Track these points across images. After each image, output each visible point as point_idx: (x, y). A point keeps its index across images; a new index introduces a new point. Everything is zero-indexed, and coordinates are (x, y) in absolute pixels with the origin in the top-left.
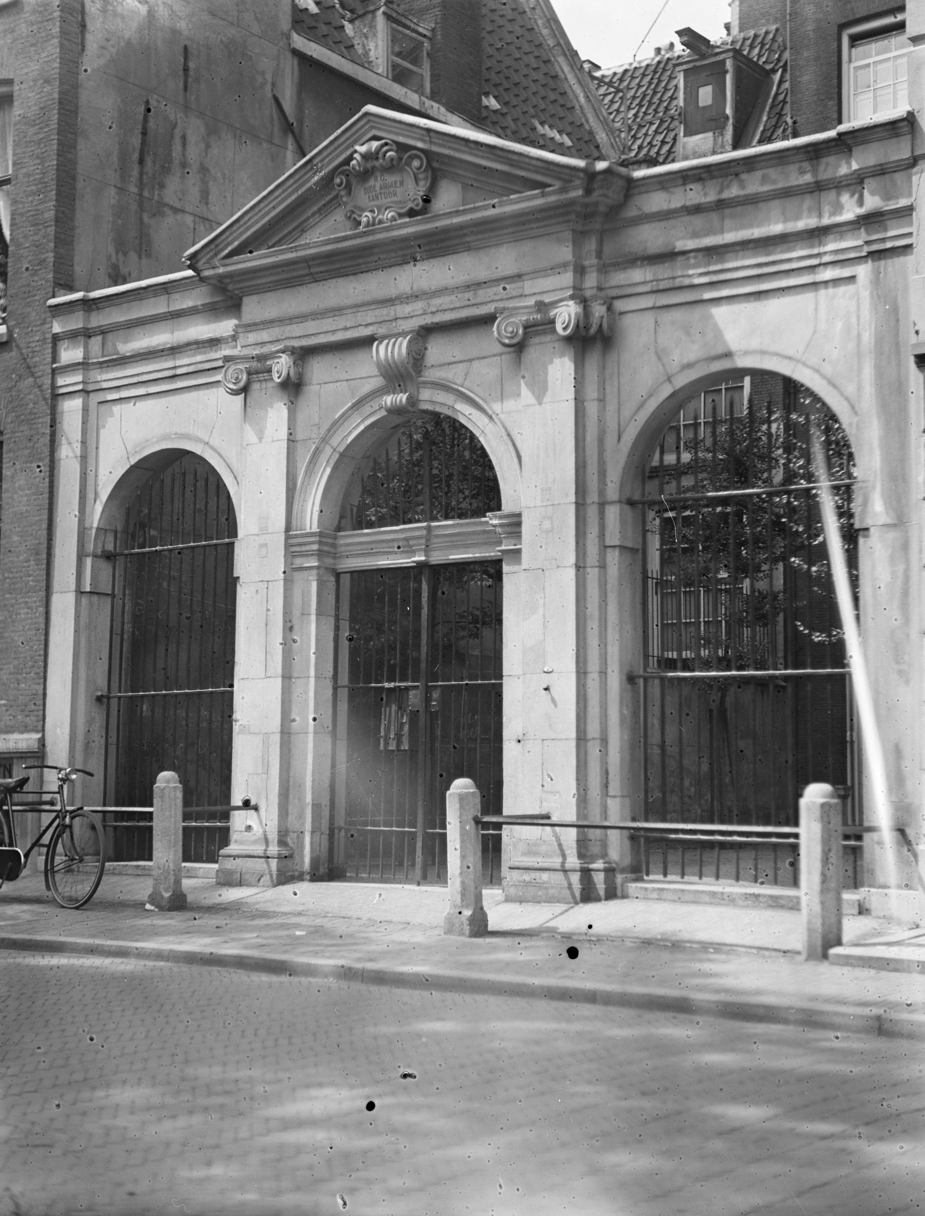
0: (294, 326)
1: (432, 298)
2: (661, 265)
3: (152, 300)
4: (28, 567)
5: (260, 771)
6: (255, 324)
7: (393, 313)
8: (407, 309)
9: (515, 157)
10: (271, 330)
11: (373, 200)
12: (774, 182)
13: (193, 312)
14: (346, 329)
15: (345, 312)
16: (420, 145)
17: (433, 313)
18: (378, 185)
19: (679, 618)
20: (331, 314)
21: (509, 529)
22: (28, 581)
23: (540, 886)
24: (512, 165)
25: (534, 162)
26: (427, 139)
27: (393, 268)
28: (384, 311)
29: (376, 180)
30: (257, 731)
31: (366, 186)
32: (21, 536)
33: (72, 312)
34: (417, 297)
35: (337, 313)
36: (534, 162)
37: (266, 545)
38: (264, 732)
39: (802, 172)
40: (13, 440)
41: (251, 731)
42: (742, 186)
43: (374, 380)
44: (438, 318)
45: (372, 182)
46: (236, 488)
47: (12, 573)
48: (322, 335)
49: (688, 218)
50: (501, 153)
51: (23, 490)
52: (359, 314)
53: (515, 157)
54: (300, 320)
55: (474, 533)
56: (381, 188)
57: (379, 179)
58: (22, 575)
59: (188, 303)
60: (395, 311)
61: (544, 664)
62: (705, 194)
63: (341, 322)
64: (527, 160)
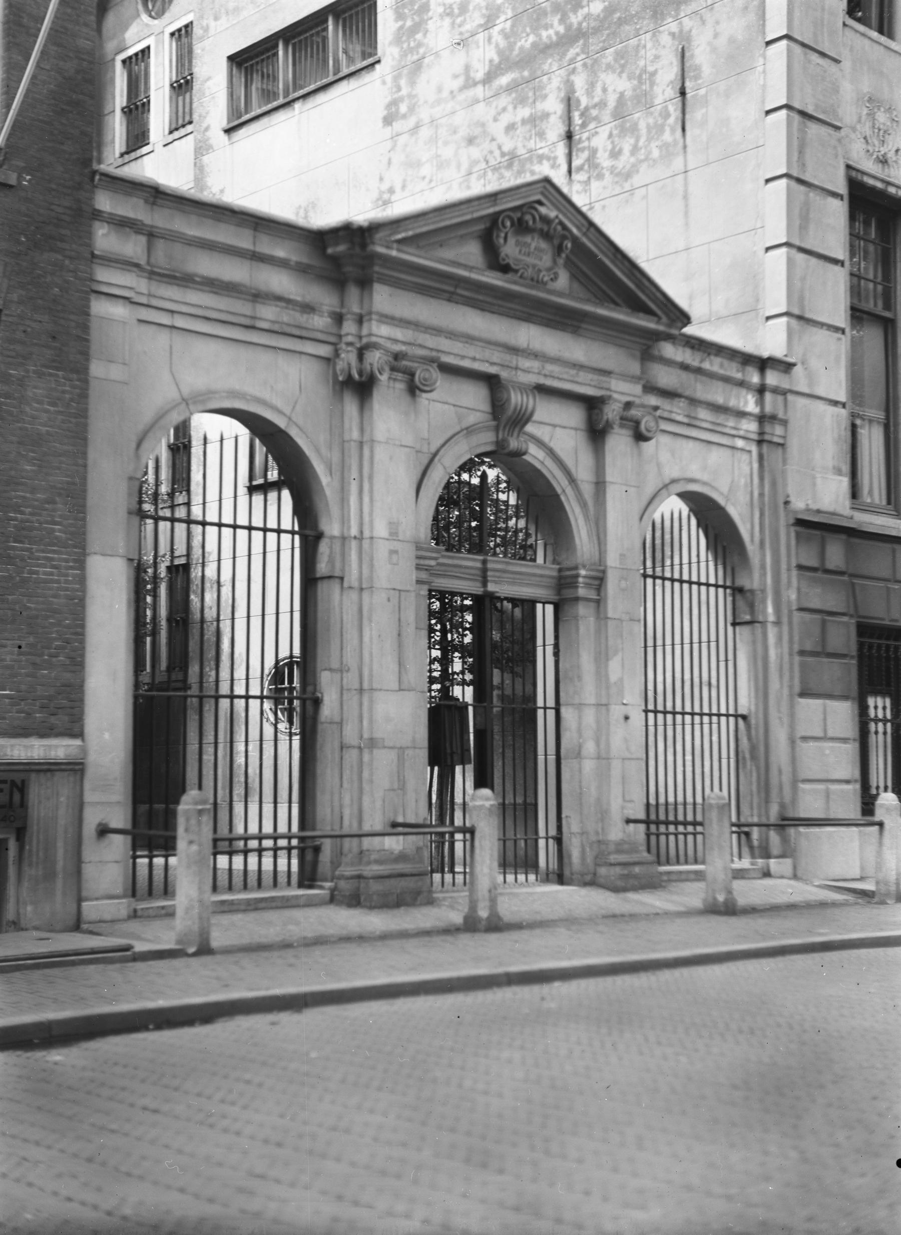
0: (428, 336)
1: (547, 362)
2: (669, 400)
3: (232, 228)
4: (54, 510)
5: (396, 786)
6: (393, 318)
7: (514, 362)
8: (526, 363)
9: (647, 283)
10: (405, 331)
11: (524, 254)
12: (726, 370)
13: (282, 264)
14: (474, 359)
15: (476, 343)
16: (575, 231)
17: (545, 376)
18: (533, 245)
19: (285, 689)
20: (464, 340)
21: (587, 581)
22: (53, 530)
23: (635, 877)
24: (637, 286)
25: (658, 294)
26: (584, 230)
27: (496, 316)
28: (508, 357)
29: (533, 239)
30: (391, 745)
31: (521, 239)
32: (40, 466)
33: (129, 194)
34: (536, 356)
35: (470, 341)
36: (658, 294)
37: (396, 552)
38: (399, 746)
39: (738, 371)
40: (22, 328)
41: (386, 744)
42: (711, 364)
43: (478, 414)
44: (549, 382)
45: (528, 239)
46: (329, 479)
47: (22, 513)
48: (452, 356)
49: (679, 372)
50: (638, 275)
51: (40, 402)
52: (487, 350)
53: (647, 283)
54: (434, 332)
55: (534, 575)
56: (535, 249)
57: (536, 239)
58: (42, 519)
59: (280, 253)
60: (517, 360)
61: (623, 698)
62: (694, 360)
63: (471, 351)
64: (654, 290)
